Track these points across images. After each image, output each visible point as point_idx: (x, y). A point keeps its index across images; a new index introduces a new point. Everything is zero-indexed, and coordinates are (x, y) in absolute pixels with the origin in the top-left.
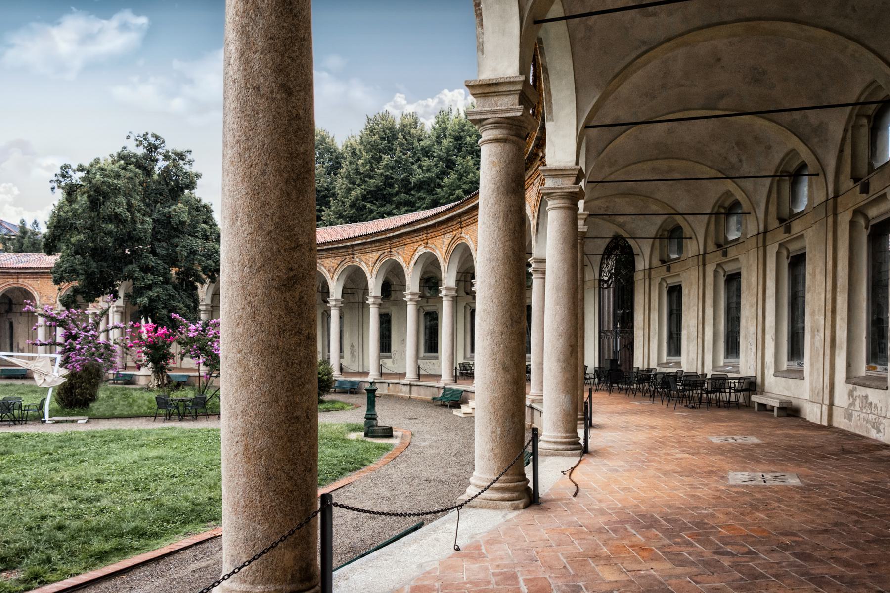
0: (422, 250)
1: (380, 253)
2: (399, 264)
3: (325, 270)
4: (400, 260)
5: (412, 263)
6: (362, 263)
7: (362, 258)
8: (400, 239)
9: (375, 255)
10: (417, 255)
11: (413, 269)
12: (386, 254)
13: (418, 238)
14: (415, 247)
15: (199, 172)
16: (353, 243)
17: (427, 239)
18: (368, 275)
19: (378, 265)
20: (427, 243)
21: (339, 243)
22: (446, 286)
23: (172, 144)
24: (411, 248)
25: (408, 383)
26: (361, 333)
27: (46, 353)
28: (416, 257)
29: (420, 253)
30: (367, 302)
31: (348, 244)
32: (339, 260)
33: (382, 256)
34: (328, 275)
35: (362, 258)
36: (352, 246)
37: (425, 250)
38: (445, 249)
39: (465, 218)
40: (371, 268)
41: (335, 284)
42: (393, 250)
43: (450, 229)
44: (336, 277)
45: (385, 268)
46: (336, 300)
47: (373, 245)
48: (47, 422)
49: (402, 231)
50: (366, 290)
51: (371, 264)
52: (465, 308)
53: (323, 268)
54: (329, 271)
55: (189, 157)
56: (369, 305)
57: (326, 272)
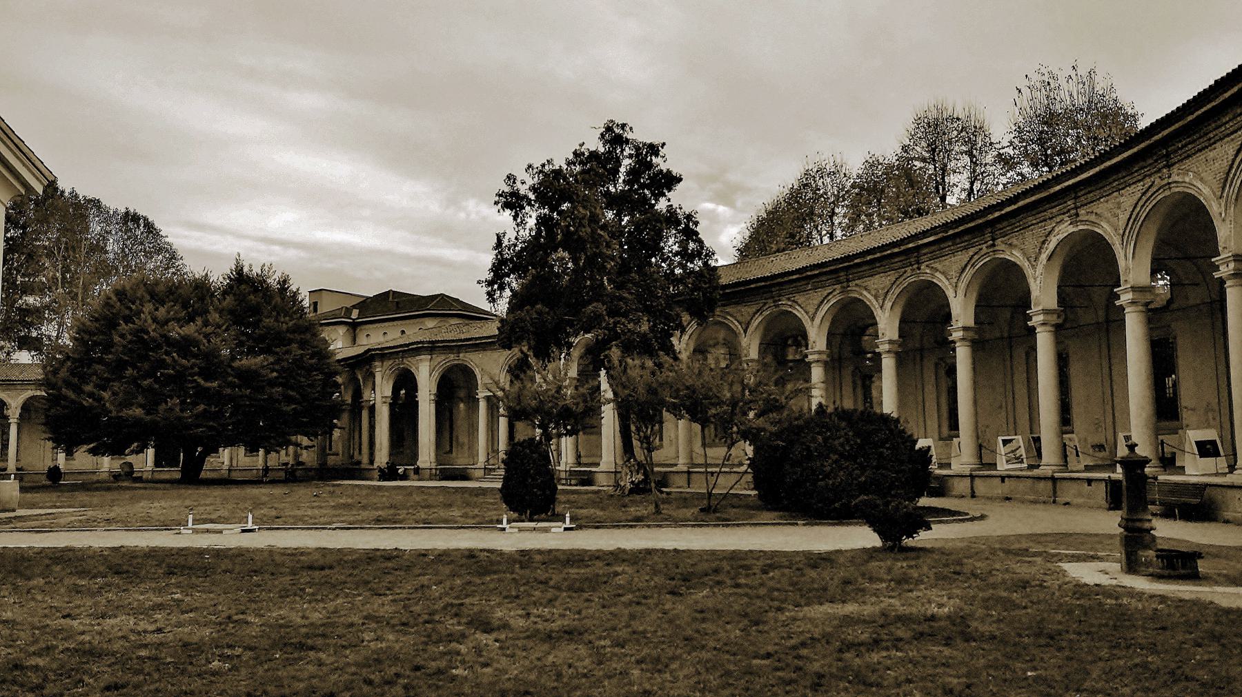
0: (1065, 229)
1: (971, 252)
2: (1015, 264)
3: (869, 296)
4: (1016, 256)
5: (1044, 257)
6: (938, 274)
7: (937, 265)
8: (1013, 221)
9: (963, 257)
10: (1053, 242)
11: (1046, 267)
12: (983, 252)
13: (1054, 210)
14: (1049, 228)
15: (675, 171)
16: (921, 242)
17: (1076, 208)
18: (950, 293)
19: (969, 273)
20: (1077, 215)
21: (894, 247)
22: (960, 325)
23: (640, 135)
24: (1039, 231)
25: (1049, 474)
26: (1106, 370)
27: (258, 455)
28: (1052, 246)
29: (1061, 237)
30: (1118, 303)
31: (911, 245)
32: (892, 276)
33: (976, 257)
34: (875, 302)
35: (937, 265)
36: (918, 248)
37: (1071, 229)
38: (1123, 217)
39: (896, 260)
40: (881, 302)
41: (887, 314)
42: (998, 242)
43: (1137, 177)
44: (888, 305)
45: (979, 281)
46: (1046, 312)
47: (958, 240)
48: (507, 531)
49: (1021, 203)
50: (1024, 301)
51: (953, 273)
52: (936, 365)
53: (865, 293)
54: (876, 297)
55: (662, 152)
56: (1122, 308)
57: (871, 298)
